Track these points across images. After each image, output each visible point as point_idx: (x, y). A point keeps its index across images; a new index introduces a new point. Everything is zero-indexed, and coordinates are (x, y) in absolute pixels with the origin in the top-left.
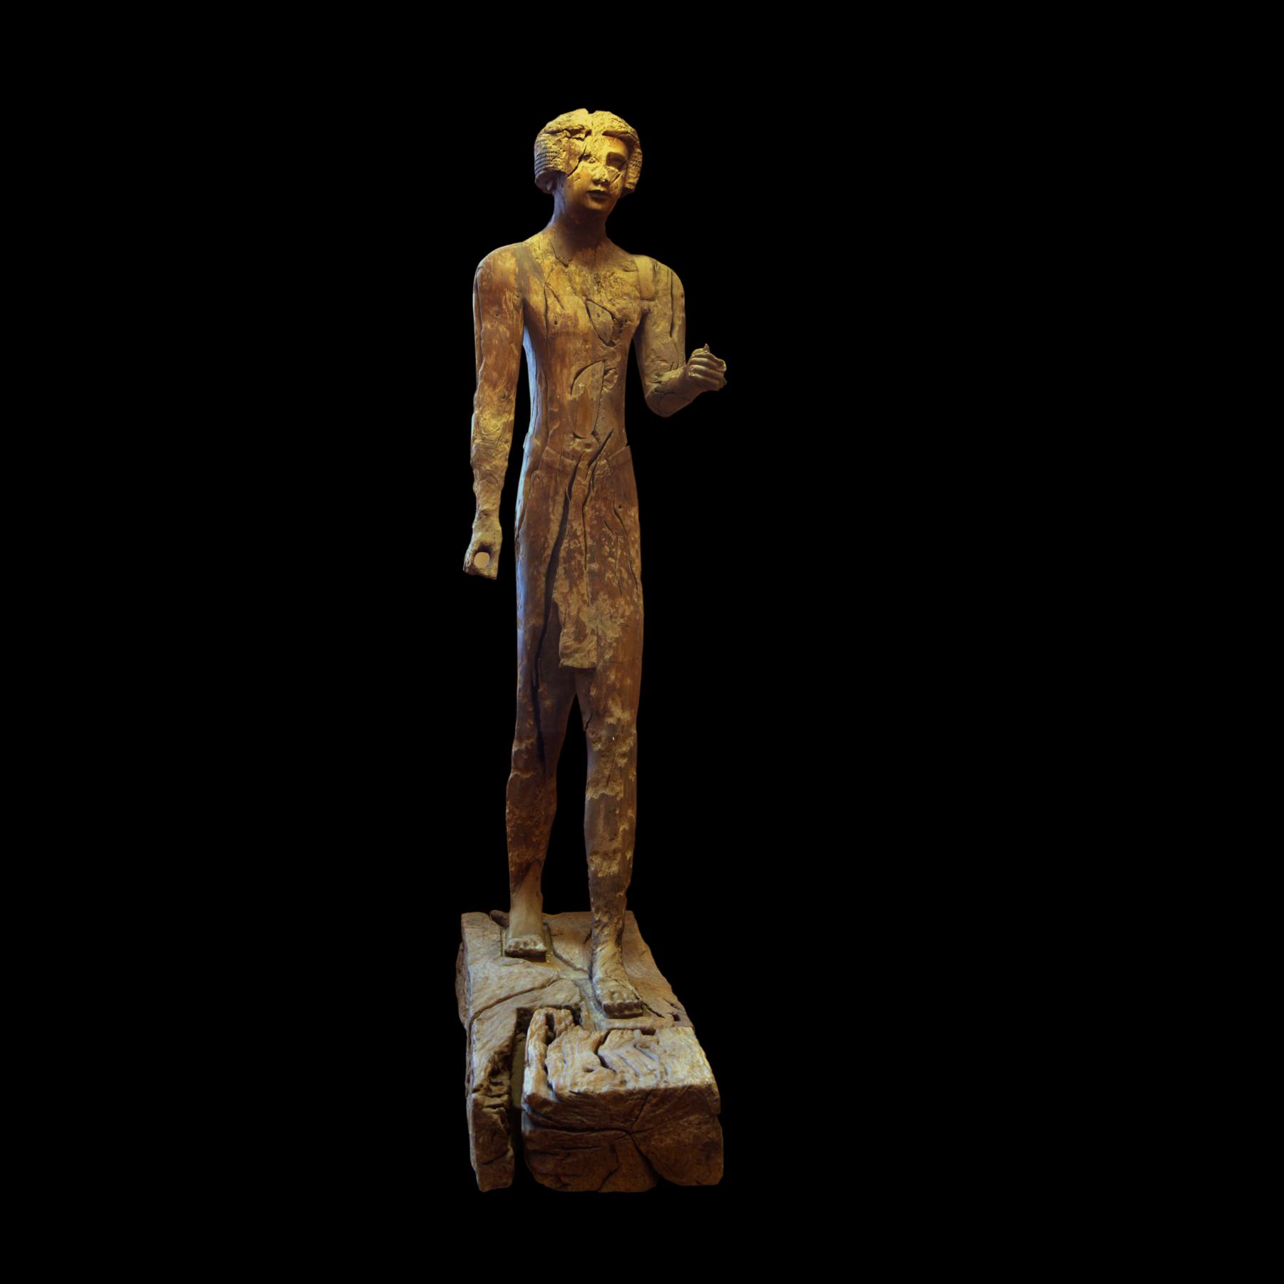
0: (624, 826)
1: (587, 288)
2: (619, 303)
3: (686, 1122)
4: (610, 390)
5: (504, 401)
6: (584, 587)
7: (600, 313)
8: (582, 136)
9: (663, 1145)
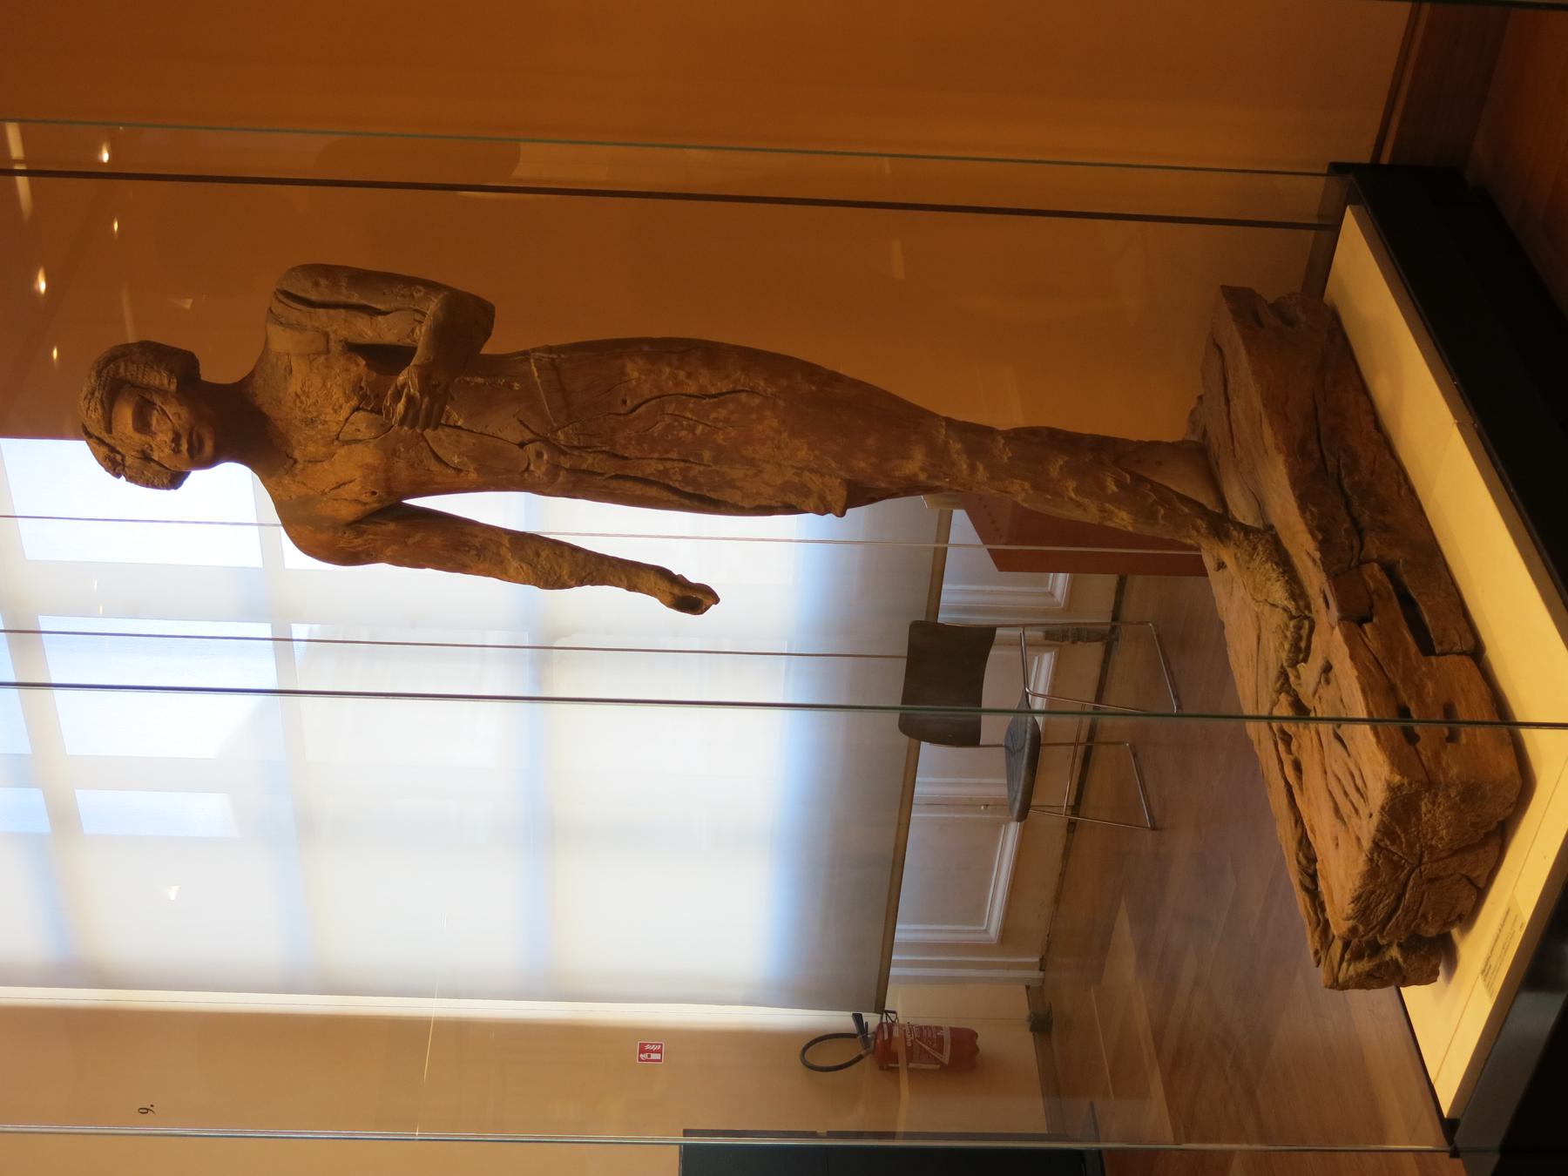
0: (1070, 489)
1: (322, 438)
2: (338, 399)
3: (1425, 815)
4: (460, 416)
5: (484, 556)
6: (737, 473)
7: (354, 428)
8: (119, 458)
9: (1446, 840)
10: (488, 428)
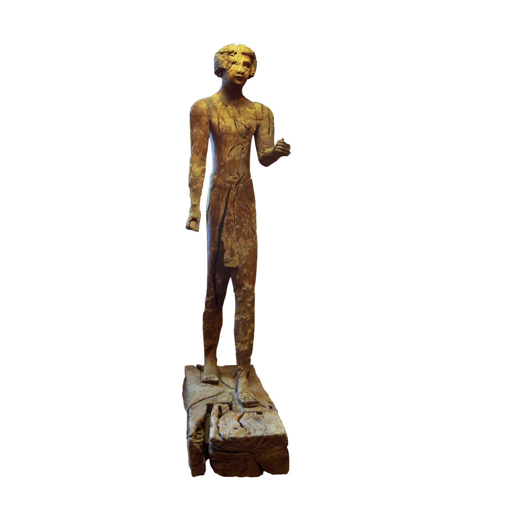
0: (250, 331)
1: (235, 115)
2: (248, 121)
3: (275, 449)
4: (244, 156)
5: (202, 161)
6: (234, 235)
7: (240, 125)
8: (233, 54)
9: (265, 458)
10: (242, 164)
